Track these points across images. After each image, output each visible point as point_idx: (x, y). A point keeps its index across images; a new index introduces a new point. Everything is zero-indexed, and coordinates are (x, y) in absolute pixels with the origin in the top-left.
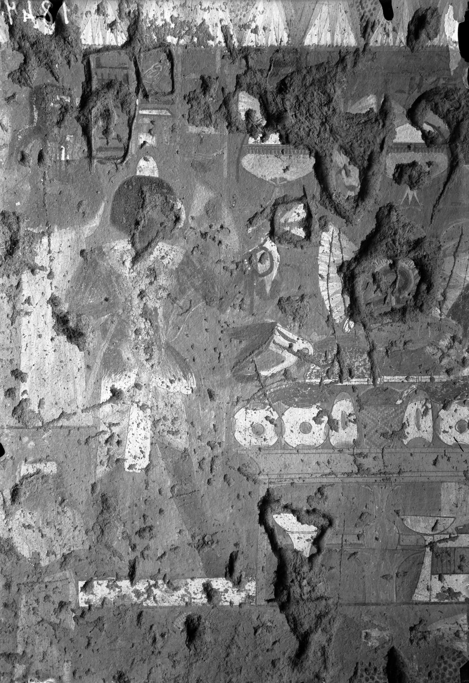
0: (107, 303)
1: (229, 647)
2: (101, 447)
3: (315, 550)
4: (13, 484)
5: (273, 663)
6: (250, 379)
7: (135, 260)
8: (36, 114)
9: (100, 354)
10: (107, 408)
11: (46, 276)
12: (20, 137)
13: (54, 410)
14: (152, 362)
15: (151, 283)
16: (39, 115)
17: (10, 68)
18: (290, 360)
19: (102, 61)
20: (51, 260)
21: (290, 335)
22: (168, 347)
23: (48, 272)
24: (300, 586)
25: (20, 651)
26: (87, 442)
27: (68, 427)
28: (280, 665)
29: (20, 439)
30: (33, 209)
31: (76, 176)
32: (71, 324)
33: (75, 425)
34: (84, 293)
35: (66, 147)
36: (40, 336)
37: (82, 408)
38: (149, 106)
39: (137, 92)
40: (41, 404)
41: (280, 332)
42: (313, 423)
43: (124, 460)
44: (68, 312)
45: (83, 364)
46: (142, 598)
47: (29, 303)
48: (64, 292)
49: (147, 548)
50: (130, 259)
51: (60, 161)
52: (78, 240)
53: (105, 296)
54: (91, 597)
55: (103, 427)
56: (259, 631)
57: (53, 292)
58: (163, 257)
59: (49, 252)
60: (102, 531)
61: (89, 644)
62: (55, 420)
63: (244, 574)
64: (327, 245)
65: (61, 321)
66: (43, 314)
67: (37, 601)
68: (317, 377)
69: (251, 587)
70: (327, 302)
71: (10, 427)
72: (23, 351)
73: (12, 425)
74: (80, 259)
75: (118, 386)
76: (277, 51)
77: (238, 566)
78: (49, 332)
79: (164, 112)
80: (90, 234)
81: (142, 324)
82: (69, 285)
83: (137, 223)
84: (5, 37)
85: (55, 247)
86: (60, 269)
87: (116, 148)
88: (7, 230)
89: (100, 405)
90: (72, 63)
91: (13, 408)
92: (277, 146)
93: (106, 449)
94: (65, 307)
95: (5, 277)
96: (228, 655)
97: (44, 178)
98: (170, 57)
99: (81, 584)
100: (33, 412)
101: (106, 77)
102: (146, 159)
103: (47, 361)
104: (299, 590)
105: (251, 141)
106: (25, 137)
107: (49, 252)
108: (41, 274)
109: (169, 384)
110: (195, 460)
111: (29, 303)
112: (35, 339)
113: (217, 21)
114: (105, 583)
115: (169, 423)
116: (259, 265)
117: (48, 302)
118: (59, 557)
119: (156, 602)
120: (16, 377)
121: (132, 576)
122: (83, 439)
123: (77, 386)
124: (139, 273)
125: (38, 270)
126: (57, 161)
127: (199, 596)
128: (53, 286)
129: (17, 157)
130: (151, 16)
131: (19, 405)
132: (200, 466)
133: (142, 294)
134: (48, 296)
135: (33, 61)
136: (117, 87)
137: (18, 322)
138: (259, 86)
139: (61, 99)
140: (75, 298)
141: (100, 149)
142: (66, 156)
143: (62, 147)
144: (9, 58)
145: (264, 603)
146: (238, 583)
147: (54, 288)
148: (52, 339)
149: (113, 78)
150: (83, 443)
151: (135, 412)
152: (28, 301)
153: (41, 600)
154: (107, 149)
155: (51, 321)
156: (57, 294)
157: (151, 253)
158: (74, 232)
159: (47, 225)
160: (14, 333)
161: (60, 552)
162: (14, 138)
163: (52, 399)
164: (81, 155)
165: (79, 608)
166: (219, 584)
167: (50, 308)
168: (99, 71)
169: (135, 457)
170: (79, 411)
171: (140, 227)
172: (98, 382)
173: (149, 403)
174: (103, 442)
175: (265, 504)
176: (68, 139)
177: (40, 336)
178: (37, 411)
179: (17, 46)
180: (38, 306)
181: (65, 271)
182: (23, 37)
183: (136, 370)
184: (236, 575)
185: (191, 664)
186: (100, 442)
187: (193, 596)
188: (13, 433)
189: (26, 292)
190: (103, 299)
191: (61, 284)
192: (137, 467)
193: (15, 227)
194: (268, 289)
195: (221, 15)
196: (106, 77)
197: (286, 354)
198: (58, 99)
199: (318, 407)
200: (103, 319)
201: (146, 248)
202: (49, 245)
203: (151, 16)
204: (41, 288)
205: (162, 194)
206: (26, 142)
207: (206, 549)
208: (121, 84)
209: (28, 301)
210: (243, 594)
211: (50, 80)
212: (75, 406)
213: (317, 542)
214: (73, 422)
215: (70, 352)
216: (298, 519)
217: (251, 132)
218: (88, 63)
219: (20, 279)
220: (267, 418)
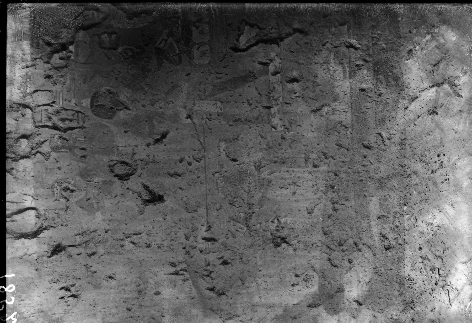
1: (299, 64)
3: (255, 27)
4: (230, 161)
5: (306, 44)
6: (180, 58)
7: (129, 109)
8: (63, 150)
10: (195, 121)
14: (174, 101)
15: (139, 102)
18: (171, 40)
19: (39, 119)
20: (129, 146)
21: (160, 40)
22: (167, 93)
24: (273, 33)
25: (303, 156)
28: (307, 41)
35: (78, 138)
38: (58, 101)
39: (52, 106)
41: (159, 45)
42: (199, 29)
43: (218, 112)
46: (279, 103)
49: (257, 101)
50: (128, 111)
51: (84, 141)
53: (145, 122)
54: (279, 125)
55: (204, 122)
56: (292, 50)
58: (127, 97)
59: (126, 146)
60: (250, 121)
61: (300, 125)
63: (267, 58)
64: (119, 25)
67: (281, 149)
68: (178, 28)
69: (273, 55)
70: (145, 24)
74: (129, 133)
75: (185, 116)
76: (33, 46)
77: (264, 61)
79: (61, 95)
81: (157, 106)
83: (112, 108)
87: (78, 116)
89: (194, 123)
90: (40, 133)
92: (75, 46)
94: (151, 140)
96: (303, 64)
98: (36, 91)
99: (273, 129)
101: (46, 119)
102: (82, 104)
104: (274, 34)
105: (72, 58)
106: (74, 155)
108: (136, 150)
109: (183, 93)
110: (216, 81)
113: (19, 71)
114: (273, 119)
115: (201, 93)
116: (129, 54)
118: (261, 140)
119: (280, 96)
120: (183, 161)
121: (269, 108)
124: (134, 107)
126: (84, 142)
127: (277, 77)
130: (19, 98)
132: (220, 78)
133: (144, 106)
135: (40, 149)
136: (50, 115)
138: (48, 54)
141: (78, 123)
145: (279, 49)
146: (271, 61)
149: (46, 116)
151: (196, 108)
152: (148, 156)
153: (281, 147)
154: (78, 120)
156: (145, 143)
157: (125, 102)
159: (113, 147)
161: (259, 139)
165: (284, 131)
166: (271, 68)
168: (43, 121)
169: (217, 108)
171: (114, 107)
172: (184, 125)
173: (192, 102)
174: (210, 122)
175: (236, 49)
176: (74, 137)
179: (33, 156)
182: (30, 153)
183: (178, 108)
184: (268, 61)
185: (307, 80)
187: (277, 80)
189: (144, 156)
192: (221, 106)
193: (115, 162)
194: (139, 50)
195: (17, 68)
196: (46, 119)
197: (169, 42)
199: (192, 27)
200: (156, 123)
201: (123, 104)
202: (122, 146)
203: (19, 98)
205: (98, 97)
207: (256, 75)
208: (49, 113)
210: (276, 58)
211: (47, 143)
213: (252, 26)
216: (242, 34)
217: (69, 57)
218: (40, 126)
220: (197, 50)
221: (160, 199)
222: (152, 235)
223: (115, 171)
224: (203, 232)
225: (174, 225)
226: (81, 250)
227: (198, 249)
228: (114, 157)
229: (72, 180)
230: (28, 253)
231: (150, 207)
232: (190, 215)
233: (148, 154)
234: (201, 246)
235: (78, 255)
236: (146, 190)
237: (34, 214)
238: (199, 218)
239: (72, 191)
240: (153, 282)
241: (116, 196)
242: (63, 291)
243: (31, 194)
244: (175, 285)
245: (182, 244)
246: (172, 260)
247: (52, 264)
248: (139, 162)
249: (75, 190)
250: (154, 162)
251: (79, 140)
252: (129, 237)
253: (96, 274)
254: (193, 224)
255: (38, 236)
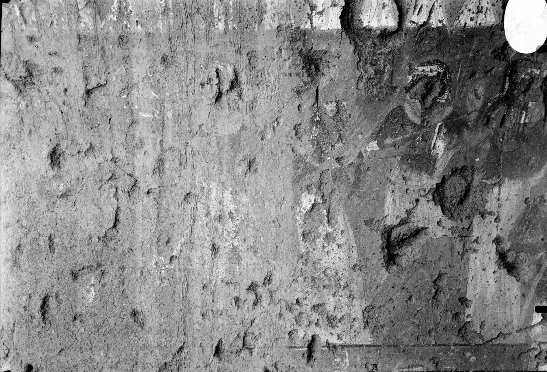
0: (543, 242)
2: (532, 361)
8: (507, 85)
9: (535, 284)
11: (493, 220)
12: (490, 104)
13: (493, 331)
16: (509, 85)
17: (495, 46)
20: (499, 207)
23: (495, 217)
26: (519, 356)
27: (503, 345)
29: (464, 355)
30: (489, 164)
31: (531, 136)
32: (510, 260)
33: (510, 343)
34: (524, 234)
35: (527, 111)
36: (484, 270)
37: (516, 329)
40: (482, 325)
44: (509, 251)
45: (519, 292)
47: (477, 243)
48: (508, 234)
51: (520, 123)
52: (525, 189)
55: (534, 345)
57: (498, 233)
59: (499, 200)
62: (493, 338)
65: (502, 256)
66: (489, 251)
71: (455, 345)
72: (469, 282)
73: (457, 342)
74: (525, 205)
78: (492, 266)
80: (535, 184)
82: (512, 227)
84: (498, 20)
85: (503, 196)
86: (506, 214)
88: (464, 182)
89: (532, 327)
91: (458, 329)
93: (536, 363)
94: (507, 246)
95: (459, 221)
97: (503, 138)
100: (475, 332)
103: (489, 290)
107: (499, 200)
108: (489, 218)
111: (477, 243)
112: (480, 273)
117: (493, 241)
122: (516, 355)
123: (513, 312)
125: (487, 215)
128: (499, 228)
129: (483, 121)
131: (463, 327)
134: (494, 236)
137: (467, 258)
139: (532, 71)
140: (517, 238)
142: (525, 120)
143: (524, 112)
144: (496, 37)
147: (499, 230)
148: (494, 272)
150: (516, 358)
152: (476, 241)
155: (494, 257)
156: (501, 235)
158: (521, 183)
160: (462, 267)
162: (484, 105)
163: (492, 322)
164: (538, 118)
167: (495, 246)
170: (514, 331)
176: (530, 105)
177: (484, 270)
178: (478, 330)
180: (484, 245)
181: (510, 215)
186: (530, 357)
188: (458, 349)
189: (475, 233)
190: (540, 239)
191: (506, 226)
193: (469, 179)
198: (529, 71)
202: (499, 194)
204: (489, 230)
206: (494, 107)
209: (476, 241)
212: (511, 327)
214: (509, 340)
215: (509, 283)
219: (472, 222)
221: (391, 259)
222: (326, 244)
223: (454, 178)
224: (325, 336)
225: (343, 284)
226: (307, 114)
227: (296, 327)
228: (480, 176)
229: (446, 100)
230: (314, 12)
231: (379, 242)
232: (360, 316)
233: (479, 240)
234: (301, 333)
235: (299, 107)
236: (411, 234)
237: (390, 25)
238: (353, 330)
239: (423, 98)
240: (236, 244)
241: (404, 179)
242: (231, 76)
243: (431, 22)
244: (228, 284)
245: (305, 298)
246: (275, 281)
247: (286, 58)
248: (466, 224)
249: (424, 104)
250: (466, 250)
251: (522, 114)
252: (324, 202)
253: (259, 138)
254: (342, 318)
255: (344, 33)
